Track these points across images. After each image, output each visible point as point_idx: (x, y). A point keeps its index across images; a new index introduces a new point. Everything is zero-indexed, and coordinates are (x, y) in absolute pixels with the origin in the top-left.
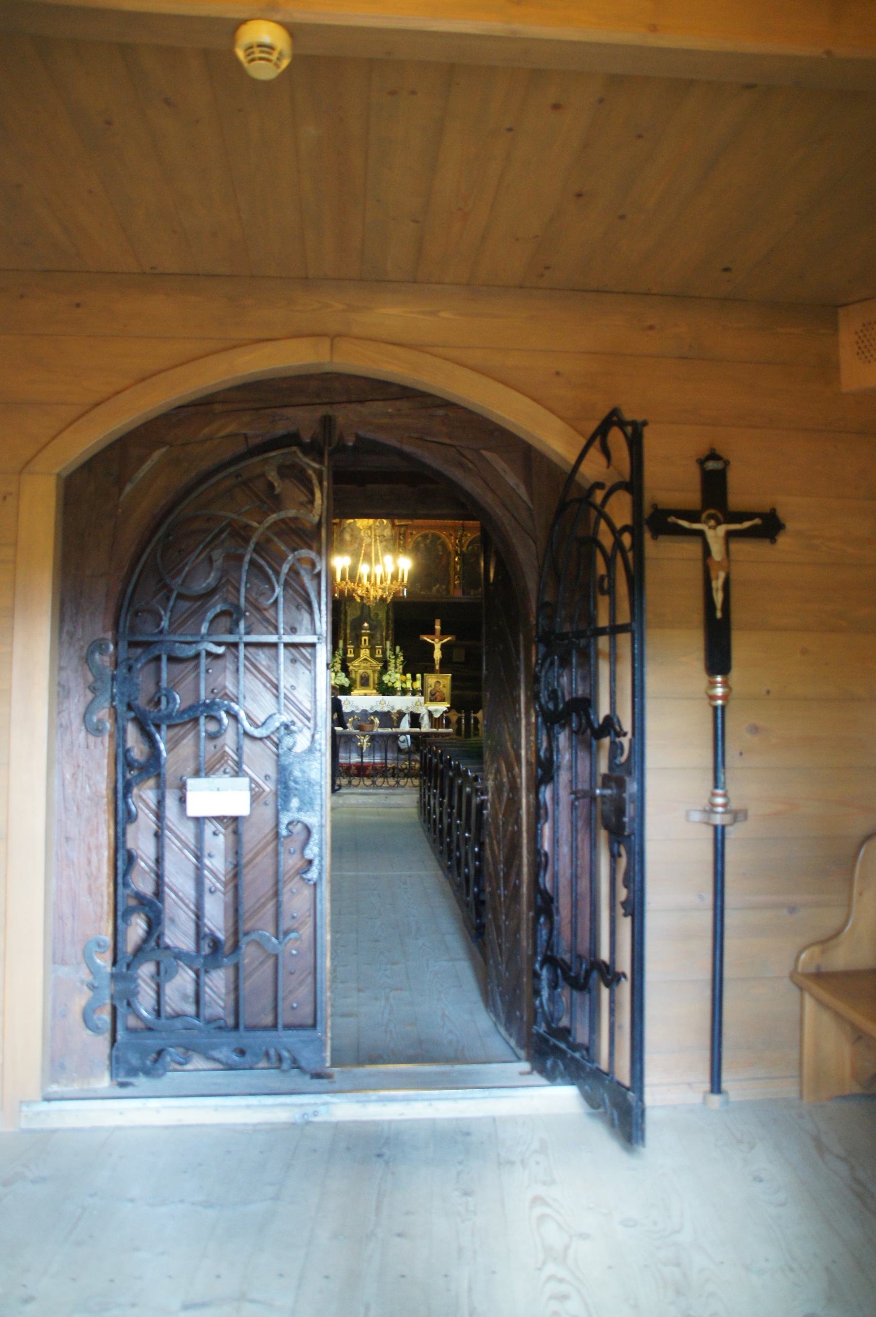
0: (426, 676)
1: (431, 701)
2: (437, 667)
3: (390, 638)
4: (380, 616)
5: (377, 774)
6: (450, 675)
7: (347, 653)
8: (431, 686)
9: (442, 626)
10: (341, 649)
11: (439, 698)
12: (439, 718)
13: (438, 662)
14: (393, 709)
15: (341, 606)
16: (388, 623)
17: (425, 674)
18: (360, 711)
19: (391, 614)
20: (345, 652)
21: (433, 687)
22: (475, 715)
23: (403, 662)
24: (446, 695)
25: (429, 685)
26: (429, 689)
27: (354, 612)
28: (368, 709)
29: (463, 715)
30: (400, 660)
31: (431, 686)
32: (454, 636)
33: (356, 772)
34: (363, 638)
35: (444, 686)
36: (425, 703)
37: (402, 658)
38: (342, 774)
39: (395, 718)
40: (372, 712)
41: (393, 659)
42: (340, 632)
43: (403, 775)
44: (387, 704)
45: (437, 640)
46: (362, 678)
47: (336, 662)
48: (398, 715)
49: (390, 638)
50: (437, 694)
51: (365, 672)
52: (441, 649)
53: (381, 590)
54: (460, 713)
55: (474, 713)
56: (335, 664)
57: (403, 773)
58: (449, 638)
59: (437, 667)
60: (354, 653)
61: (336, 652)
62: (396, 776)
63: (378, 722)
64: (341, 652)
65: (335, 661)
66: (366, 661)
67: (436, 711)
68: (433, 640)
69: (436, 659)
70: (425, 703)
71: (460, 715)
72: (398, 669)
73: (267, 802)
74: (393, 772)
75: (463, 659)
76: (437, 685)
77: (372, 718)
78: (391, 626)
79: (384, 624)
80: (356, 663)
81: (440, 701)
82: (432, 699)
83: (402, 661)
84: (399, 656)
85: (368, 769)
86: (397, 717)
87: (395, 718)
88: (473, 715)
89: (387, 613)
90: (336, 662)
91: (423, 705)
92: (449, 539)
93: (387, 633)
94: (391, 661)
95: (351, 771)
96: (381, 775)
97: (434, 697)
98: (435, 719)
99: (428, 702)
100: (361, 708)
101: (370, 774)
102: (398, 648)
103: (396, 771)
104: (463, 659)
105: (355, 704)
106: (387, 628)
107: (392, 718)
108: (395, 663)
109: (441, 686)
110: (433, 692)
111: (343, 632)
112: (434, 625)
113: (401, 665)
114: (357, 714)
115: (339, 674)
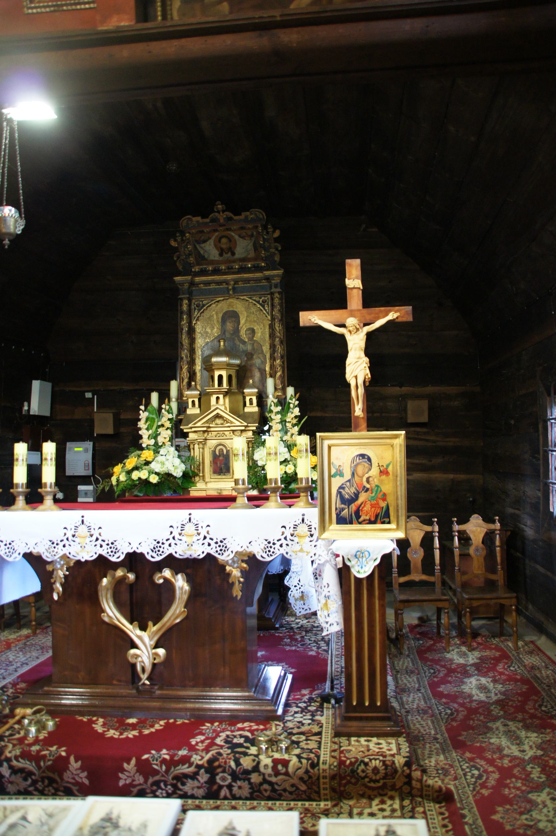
0: (322, 439)
1: (341, 520)
2: (358, 410)
3: (279, 374)
4: (258, 336)
5: (157, 784)
6: (403, 432)
7: (186, 408)
8: (340, 473)
9: (365, 277)
10: (174, 400)
11: (367, 512)
12: (370, 577)
13: (361, 391)
14: (224, 549)
15: (182, 319)
16: (273, 347)
17: (318, 434)
18: (122, 557)
19: (278, 327)
20: (182, 408)
21: (348, 475)
22: (463, 527)
23: (300, 418)
24: (391, 500)
25: (333, 471)
26: (337, 483)
27: (209, 330)
28: (145, 549)
29: (436, 528)
30: (293, 415)
31: (340, 473)
32: (410, 308)
33: (83, 777)
34: (217, 374)
35: (384, 472)
36: (323, 527)
37: (297, 412)
38: (40, 785)
39: (236, 573)
40: (158, 559)
41: (277, 413)
42: (181, 369)
43: (246, 792)
44: (203, 532)
45: (351, 322)
46: (215, 458)
47: (163, 426)
48: (245, 565)
49: (279, 374)
50: (363, 497)
51: (220, 445)
52: (368, 351)
53: (225, 255)
54: (431, 524)
55: (459, 523)
56: (160, 430)
57: (245, 784)
58: (392, 316)
59: (358, 410)
60: (200, 406)
61: (163, 406)
62: (224, 792)
63: (186, 587)
64: (174, 405)
65: (160, 423)
66: (218, 421)
67: (359, 555)
68: (343, 326)
69: (353, 384)
70: (323, 527)
71: (429, 528)
72: (289, 434)
73: (384, 477)
74: (212, 781)
75: (424, 419)
76: (360, 470)
77: (167, 573)
78: (280, 349)
79: (266, 348)
80: (199, 424)
81: (370, 522)
82: (345, 513)
83: (296, 417)
84: (292, 406)
85: (123, 770)
86: (244, 573)
87: (236, 573)
88: (456, 527)
89: (272, 327)
90: (163, 426)
91: (316, 533)
92: (437, 817)
93: (272, 367)
94: (273, 416)
95: (67, 776)
96: (170, 789)
97: (353, 507)
98: (359, 581)
99: (334, 526)
100: (124, 549)
101: (131, 785)
102: (290, 391)
103: (220, 778)
104: (424, 419)
105: (108, 536)
106: (273, 358)
107: (229, 575)
108: (283, 422)
109: (374, 471)
110: (349, 492)
111: (185, 368)
112: (342, 275)
113: (294, 425)
114: (115, 566)
115: (162, 451)
